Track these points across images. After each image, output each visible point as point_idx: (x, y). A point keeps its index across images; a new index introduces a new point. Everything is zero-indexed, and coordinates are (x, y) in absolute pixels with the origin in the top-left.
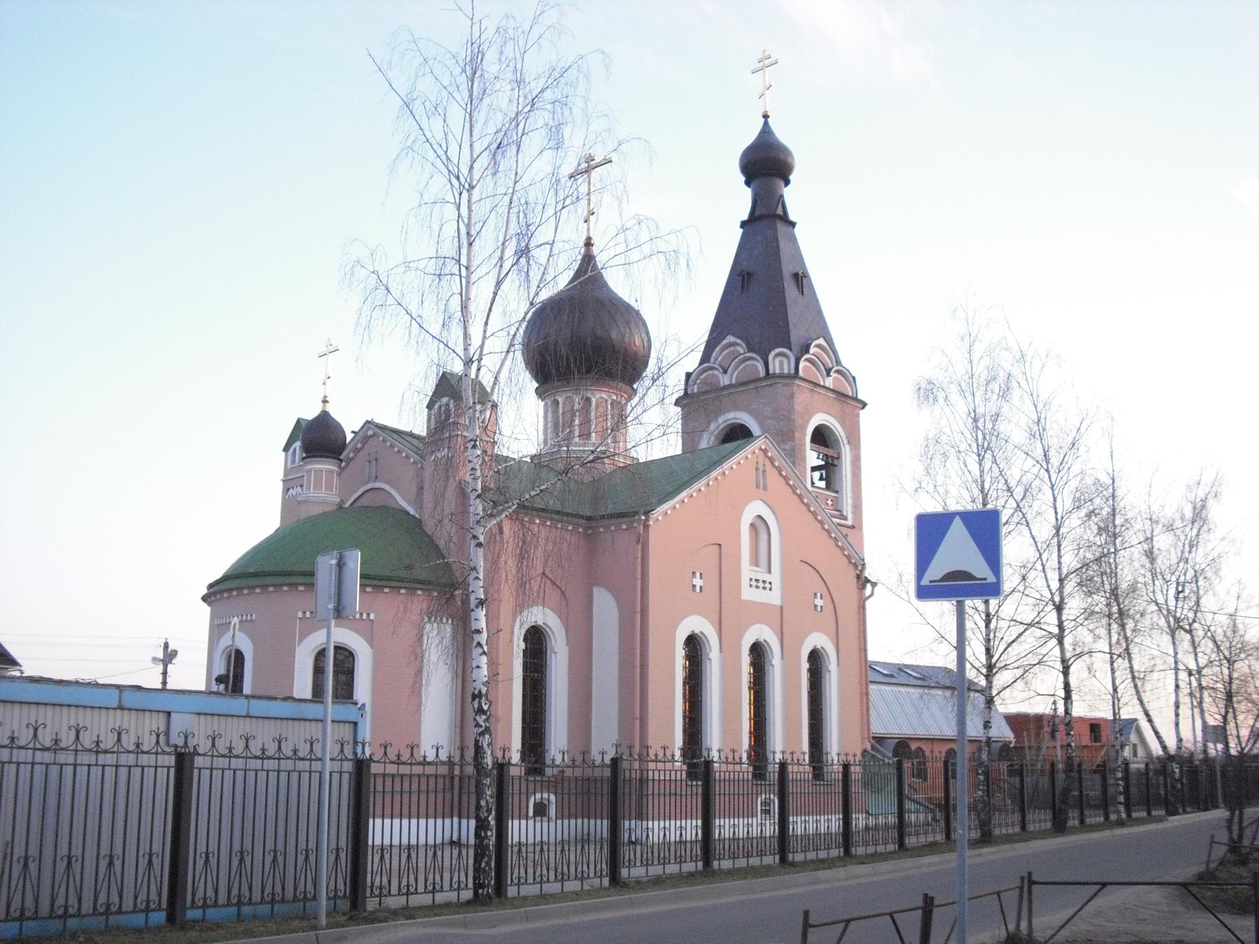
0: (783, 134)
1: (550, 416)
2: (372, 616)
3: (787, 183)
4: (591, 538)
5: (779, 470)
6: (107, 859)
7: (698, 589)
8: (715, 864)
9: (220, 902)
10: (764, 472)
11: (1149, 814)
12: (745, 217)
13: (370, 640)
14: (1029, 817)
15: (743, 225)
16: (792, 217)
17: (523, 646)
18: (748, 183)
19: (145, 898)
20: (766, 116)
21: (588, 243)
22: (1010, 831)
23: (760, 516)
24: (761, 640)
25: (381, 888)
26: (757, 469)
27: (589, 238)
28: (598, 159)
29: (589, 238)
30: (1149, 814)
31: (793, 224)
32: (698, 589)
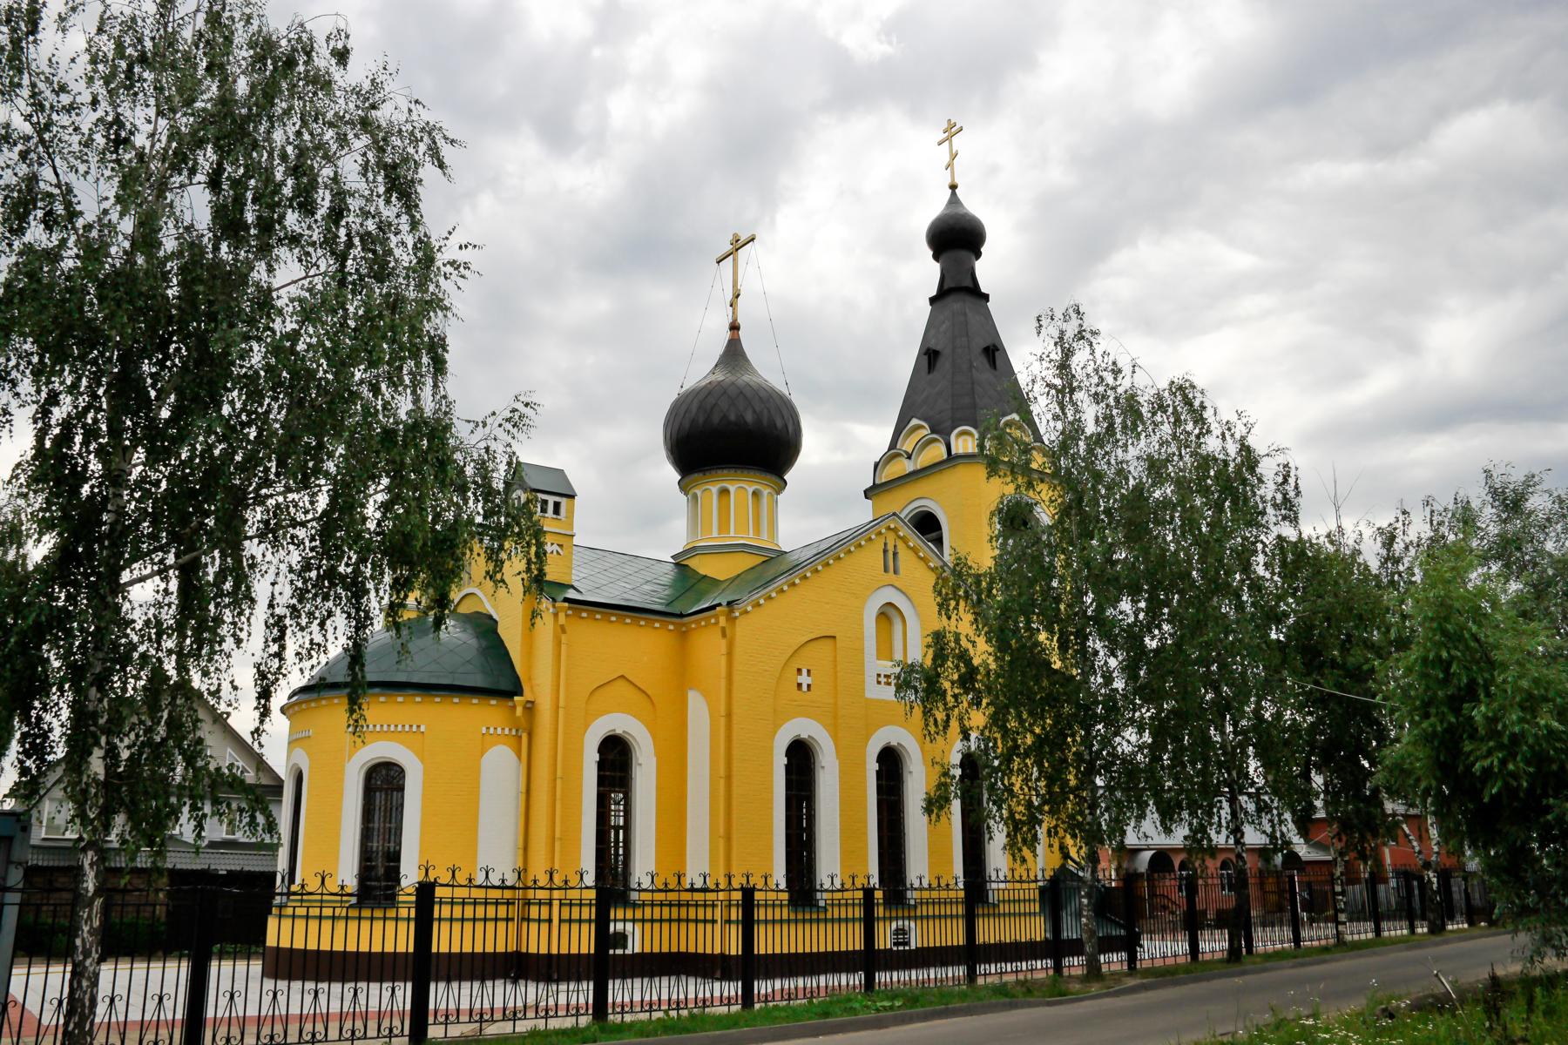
0: (975, 205)
1: (835, 540)
2: (423, 728)
3: (978, 255)
4: (683, 635)
5: (914, 550)
6: (107, 1000)
7: (805, 688)
8: (1066, 972)
9: (369, 1034)
10: (895, 554)
11: (1378, 931)
12: (934, 293)
13: (421, 755)
14: (1305, 933)
15: (933, 300)
16: (984, 290)
17: (876, 766)
18: (936, 257)
19: (153, 1038)
20: (953, 187)
21: (734, 327)
22: (1363, 937)
23: (890, 604)
24: (894, 743)
25: (704, 1001)
26: (885, 551)
27: (735, 321)
28: (743, 239)
29: (735, 321)
30: (1378, 931)
31: (986, 297)
32: (805, 688)
